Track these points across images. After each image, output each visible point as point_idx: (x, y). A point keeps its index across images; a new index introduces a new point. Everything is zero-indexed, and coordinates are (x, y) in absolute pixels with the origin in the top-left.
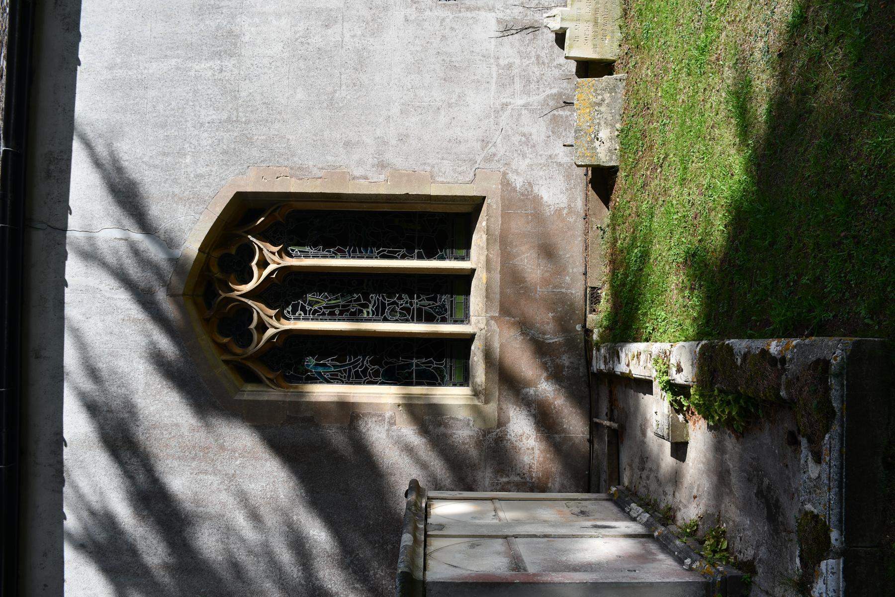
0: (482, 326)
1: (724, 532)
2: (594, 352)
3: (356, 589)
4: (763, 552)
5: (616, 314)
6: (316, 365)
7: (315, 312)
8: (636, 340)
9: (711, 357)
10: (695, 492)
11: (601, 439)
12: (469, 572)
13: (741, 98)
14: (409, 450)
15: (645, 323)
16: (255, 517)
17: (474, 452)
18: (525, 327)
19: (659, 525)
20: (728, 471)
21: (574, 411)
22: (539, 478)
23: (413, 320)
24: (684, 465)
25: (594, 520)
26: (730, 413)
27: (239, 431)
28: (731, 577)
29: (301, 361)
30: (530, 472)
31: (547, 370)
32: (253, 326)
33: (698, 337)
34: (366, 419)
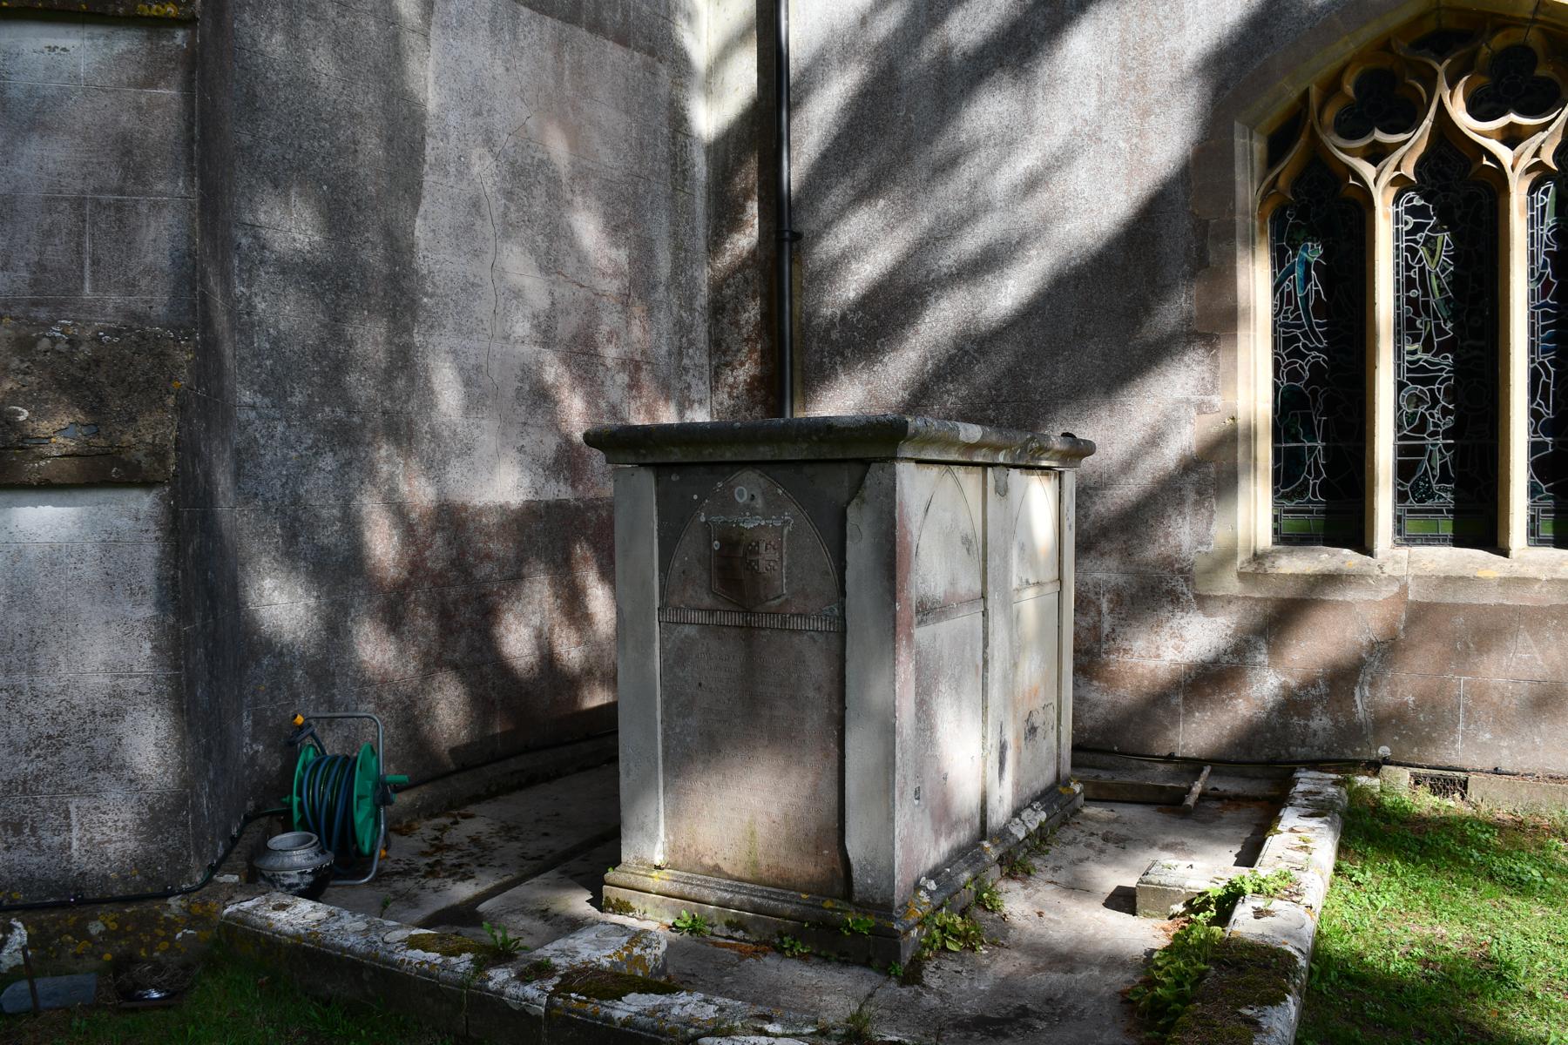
0: (1388, 569)
1: (973, 949)
2: (1334, 776)
3: (925, 363)
4: (931, 1000)
5: (1404, 822)
6: (1307, 264)
7: (1413, 251)
8: (1342, 850)
9: (1267, 967)
10: (1048, 915)
11: (1175, 776)
12: (915, 532)
13: (243, 461)
14: (1155, 439)
15: (1373, 869)
16: (1032, 184)
17: (1152, 553)
18: (1388, 649)
19: (1001, 850)
20: (1072, 971)
21: (1225, 732)
22: (1107, 664)
23: (1400, 439)
24: (1099, 904)
25: (1019, 748)
26: (1162, 984)
27: (1177, 139)
28: (898, 947)
29: (1313, 235)
30: (1118, 650)
31: (1302, 687)
32: (1380, 136)
33: (1318, 954)
34: (1207, 361)
